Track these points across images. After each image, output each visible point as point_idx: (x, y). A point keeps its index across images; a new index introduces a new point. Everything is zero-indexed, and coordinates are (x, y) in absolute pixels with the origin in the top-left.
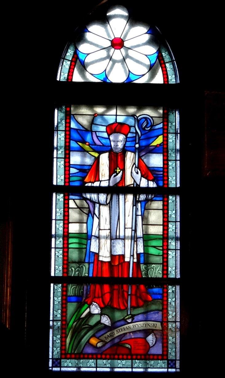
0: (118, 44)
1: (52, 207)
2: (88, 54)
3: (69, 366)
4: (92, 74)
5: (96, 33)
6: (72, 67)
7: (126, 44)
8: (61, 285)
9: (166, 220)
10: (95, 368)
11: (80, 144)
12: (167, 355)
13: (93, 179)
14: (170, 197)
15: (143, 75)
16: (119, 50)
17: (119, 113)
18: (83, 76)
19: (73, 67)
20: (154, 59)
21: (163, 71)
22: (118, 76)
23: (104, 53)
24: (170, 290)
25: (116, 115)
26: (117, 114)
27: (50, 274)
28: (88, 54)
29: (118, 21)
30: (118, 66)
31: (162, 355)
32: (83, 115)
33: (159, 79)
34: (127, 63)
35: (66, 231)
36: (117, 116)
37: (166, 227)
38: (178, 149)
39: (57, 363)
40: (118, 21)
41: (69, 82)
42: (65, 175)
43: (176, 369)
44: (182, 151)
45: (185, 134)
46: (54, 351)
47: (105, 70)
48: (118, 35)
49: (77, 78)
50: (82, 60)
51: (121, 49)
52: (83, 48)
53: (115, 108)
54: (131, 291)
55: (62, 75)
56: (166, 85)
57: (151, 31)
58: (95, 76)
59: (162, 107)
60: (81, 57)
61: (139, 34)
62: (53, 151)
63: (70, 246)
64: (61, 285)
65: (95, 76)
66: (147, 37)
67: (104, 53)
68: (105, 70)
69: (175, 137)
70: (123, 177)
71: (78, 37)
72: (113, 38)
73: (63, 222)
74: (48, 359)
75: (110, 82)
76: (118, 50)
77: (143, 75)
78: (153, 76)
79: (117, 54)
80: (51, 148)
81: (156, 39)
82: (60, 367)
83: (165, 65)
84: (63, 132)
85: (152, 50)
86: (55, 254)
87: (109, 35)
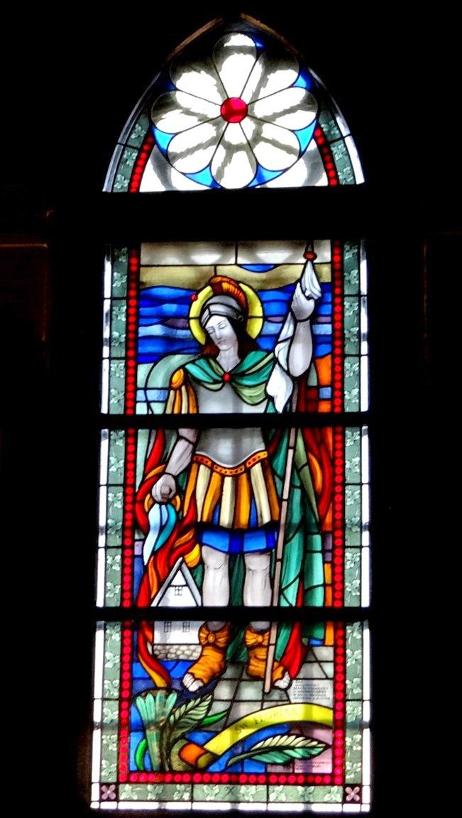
3: (134, 798)
5: (194, 88)
7: (260, 110)
8: (123, 432)
11: (244, 733)
12: (343, 775)
13: (193, 408)
14: (348, 433)
16: (238, 124)
18: (164, 177)
22: (237, 177)
23: (209, 131)
27: (95, 602)
29: (240, 68)
30: (241, 157)
31: (332, 775)
32: (169, 267)
34: (210, 159)
38: (364, 334)
40: (240, 68)
41: (134, 197)
42: (122, 584)
45: (379, 301)
46: (101, 766)
47: (210, 165)
49: (151, 183)
50: (163, 149)
51: (242, 122)
52: (167, 123)
54: (122, 140)
55: (116, 182)
56: (337, 191)
58: (188, 176)
60: (162, 140)
61: (284, 90)
64: (123, 432)
66: (300, 94)
67: (209, 131)
68: (210, 165)
69: (357, 304)
70: (306, 501)
76: (237, 119)
79: (236, 133)
80: (98, 342)
81: (319, 99)
84: (121, 361)
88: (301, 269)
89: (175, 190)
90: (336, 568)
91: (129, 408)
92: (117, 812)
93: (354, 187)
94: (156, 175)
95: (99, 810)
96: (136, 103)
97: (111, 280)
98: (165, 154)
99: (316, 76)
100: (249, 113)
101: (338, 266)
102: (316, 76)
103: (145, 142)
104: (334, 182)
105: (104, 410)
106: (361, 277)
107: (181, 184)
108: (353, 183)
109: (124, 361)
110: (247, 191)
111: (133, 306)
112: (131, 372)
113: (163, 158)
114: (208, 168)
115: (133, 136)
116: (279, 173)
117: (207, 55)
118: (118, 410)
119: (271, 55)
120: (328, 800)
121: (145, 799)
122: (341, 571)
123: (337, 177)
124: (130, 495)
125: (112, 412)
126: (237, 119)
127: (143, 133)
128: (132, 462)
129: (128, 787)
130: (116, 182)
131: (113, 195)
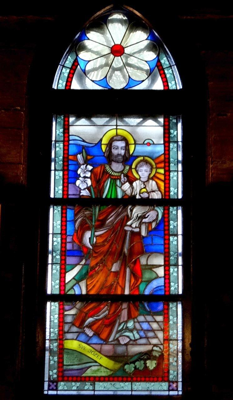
0: (117, 50)
1: (50, 187)
2: (89, 61)
3: (64, 389)
4: (93, 81)
5: (95, 41)
6: (71, 75)
7: (127, 51)
9: (167, 246)
10: (93, 392)
15: (143, 81)
17: (119, 123)
19: (72, 76)
20: (154, 64)
21: (162, 78)
22: (118, 83)
23: (103, 61)
24: (172, 287)
25: (117, 126)
26: (118, 125)
28: (89, 61)
29: (116, 30)
32: (82, 129)
33: (158, 85)
35: (68, 83)
36: (116, 124)
37: (167, 245)
39: (54, 383)
40: (116, 30)
41: (68, 91)
43: (178, 391)
44: (185, 162)
48: (118, 42)
49: (75, 85)
52: (83, 55)
53: (116, 119)
55: (59, 84)
56: (167, 92)
57: (152, 37)
58: (95, 82)
59: (163, 116)
62: (47, 257)
63: (70, 142)
65: (95, 82)
71: (78, 46)
72: (113, 44)
73: (60, 237)
74: (43, 381)
75: (110, 88)
76: (117, 53)
77: (143, 81)
78: (153, 81)
79: (118, 62)
81: (155, 46)
82: (57, 390)
83: (164, 71)
85: (151, 56)
86: (53, 224)
87: (107, 41)
88: (151, 130)
89: (88, 89)
90: (168, 282)
91: (66, 187)
92: (57, 395)
93: (176, 91)
94: (76, 82)
95: (47, 394)
96: (65, 51)
97: (56, 131)
98: (84, 72)
99: (156, 34)
100: (110, 49)
101: (167, 127)
102: (156, 34)
103: (73, 65)
104: (166, 88)
105: (52, 196)
106: (178, 132)
107: (90, 86)
108: (176, 89)
109: (63, 142)
110: (123, 91)
111: (66, 137)
112: (63, 275)
113: (82, 73)
114: (105, 78)
115: (67, 62)
116: (140, 82)
117: (100, 24)
118: (60, 194)
119: (133, 24)
120: (160, 388)
121: (71, 389)
122: (166, 280)
123: (168, 85)
124: (66, 183)
125: (57, 197)
126: (117, 53)
127: (72, 61)
128: (65, 175)
129: (62, 383)
130: (59, 84)
131: (58, 91)
